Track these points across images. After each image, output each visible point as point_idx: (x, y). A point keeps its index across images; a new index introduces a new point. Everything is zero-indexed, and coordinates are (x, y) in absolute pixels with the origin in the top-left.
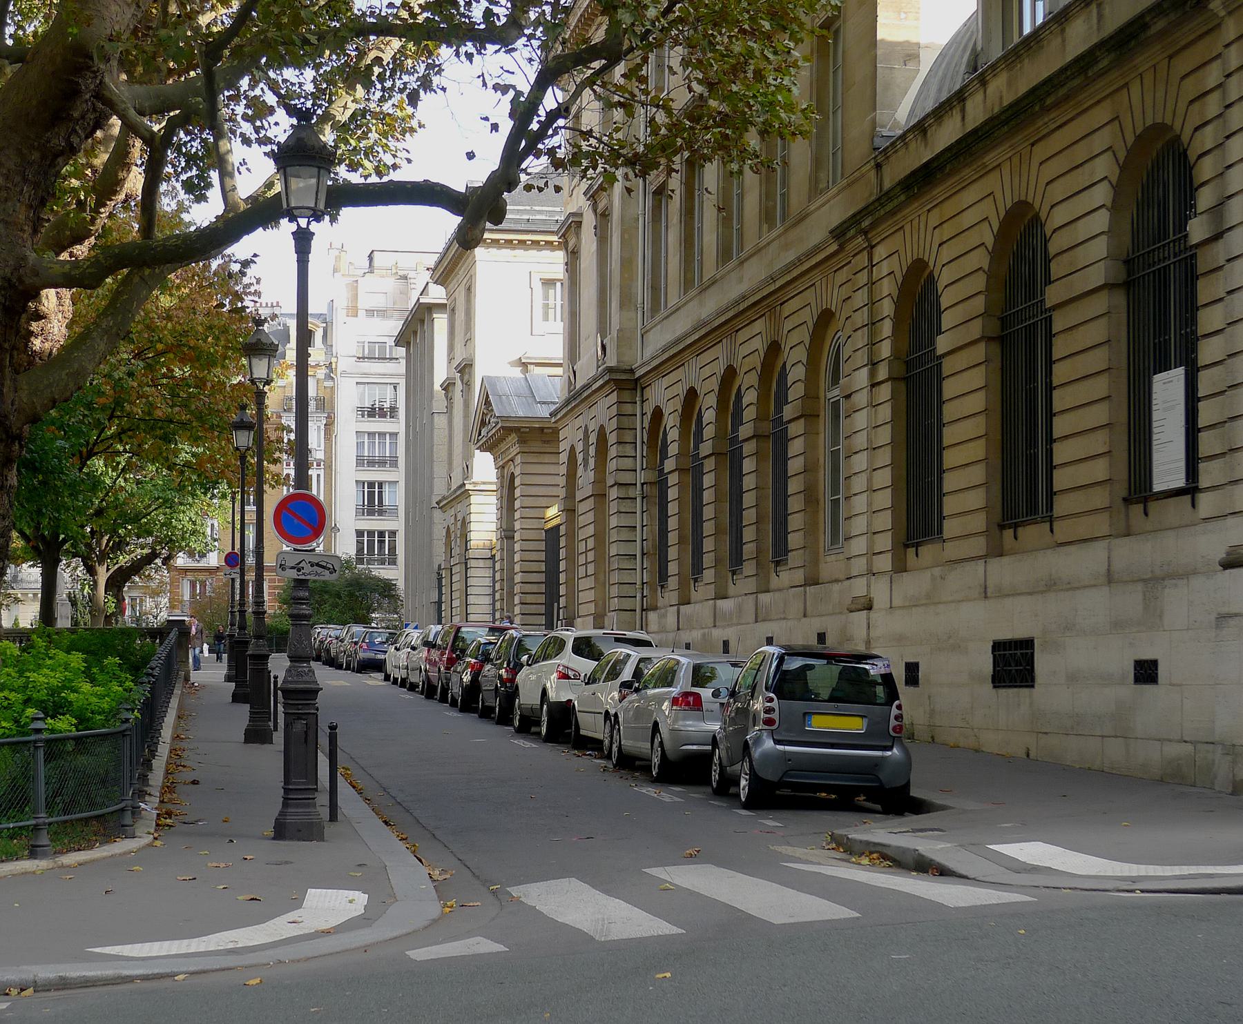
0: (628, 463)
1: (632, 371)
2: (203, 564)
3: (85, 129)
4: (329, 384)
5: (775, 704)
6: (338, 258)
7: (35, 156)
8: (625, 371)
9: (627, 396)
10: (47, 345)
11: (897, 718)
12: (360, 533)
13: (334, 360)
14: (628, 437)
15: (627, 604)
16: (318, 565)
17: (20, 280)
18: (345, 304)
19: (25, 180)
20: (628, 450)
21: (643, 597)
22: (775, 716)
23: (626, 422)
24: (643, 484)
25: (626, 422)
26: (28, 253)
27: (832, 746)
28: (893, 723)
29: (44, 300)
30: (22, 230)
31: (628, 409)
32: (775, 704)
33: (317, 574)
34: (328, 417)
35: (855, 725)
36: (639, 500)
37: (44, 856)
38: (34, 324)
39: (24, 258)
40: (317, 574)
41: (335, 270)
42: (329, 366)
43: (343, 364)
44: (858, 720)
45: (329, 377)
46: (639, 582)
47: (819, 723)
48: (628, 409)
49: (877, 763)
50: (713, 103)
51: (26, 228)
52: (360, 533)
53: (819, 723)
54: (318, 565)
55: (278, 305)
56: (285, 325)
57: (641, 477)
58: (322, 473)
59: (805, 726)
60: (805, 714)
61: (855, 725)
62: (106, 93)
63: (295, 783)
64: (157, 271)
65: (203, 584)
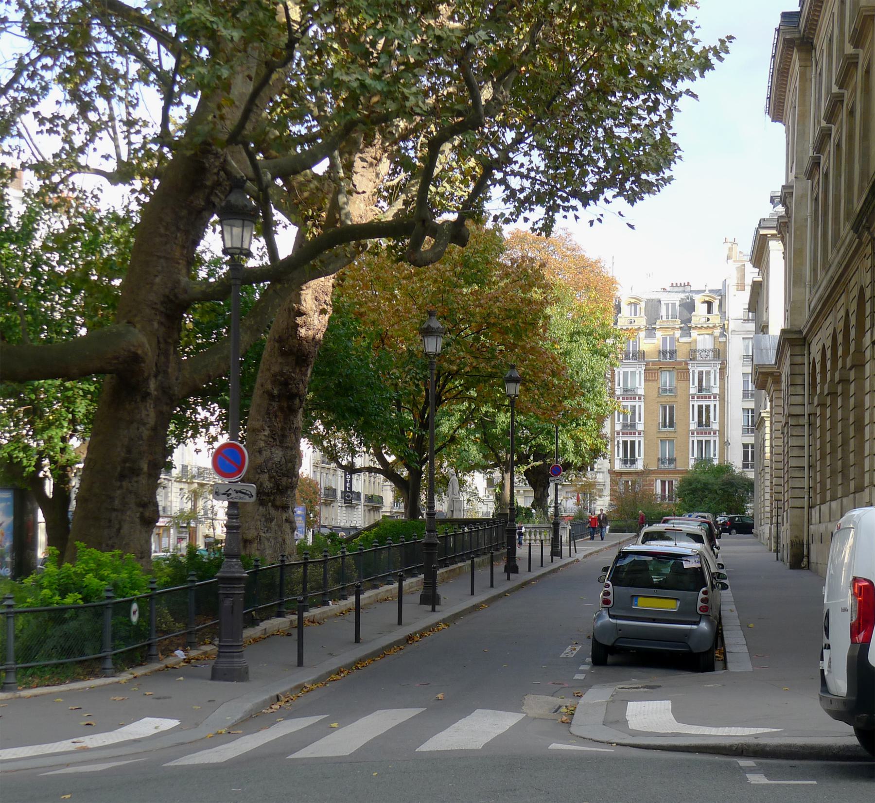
0: (798, 400)
1: (801, 332)
2: (633, 469)
3: (222, 192)
4: (722, 339)
5: (610, 589)
6: (731, 249)
7: (184, 213)
8: (796, 332)
9: (797, 350)
10: (310, 333)
11: (703, 601)
12: (745, 446)
13: (726, 322)
14: (798, 380)
15: (798, 503)
16: (240, 492)
17: (176, 296)
18: (735, 281)
19: (178, 229)
20: (799, 390)
21: (810, 498)
22: (611, 598)
23: (797, 369)
24: (809, 415)
25: (797, 369)
26: (182, 278)
27: (654, 621)
28: (700, 604)
29: (303, 302)
30: (179, 263)
31: (798, 360)
32: (610, 589)
33: (241, 498)
34: (722, 363)
35: (671, 606)
36: (806, 427)
37: (10, 690)
38: (298, 319)
39: (178, 282)
40: (241, 498)
41: (729, 258)
42: (723, 328)
43: (732, 326)
44: (673, 602)
45: (723, 335)
46: (806, 487)
47: (644, 603)
48: (798, 360)
49: (687, 634)
50: (566, 150)
51: (181, 261)
52: (745, 446)
53: (644, 603)
54: (240, 492)
55: (688, 284)
56: (691, 299)
57: (807, 410)
58: (717, 404)
59: (632, 605)
60: (633, 596)
61: (671, 606)
62: (228, 168)
63: (226, 642)
64: (286, 285)
65: (671, 482)
